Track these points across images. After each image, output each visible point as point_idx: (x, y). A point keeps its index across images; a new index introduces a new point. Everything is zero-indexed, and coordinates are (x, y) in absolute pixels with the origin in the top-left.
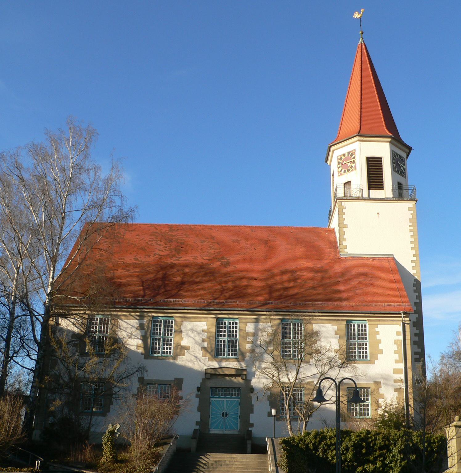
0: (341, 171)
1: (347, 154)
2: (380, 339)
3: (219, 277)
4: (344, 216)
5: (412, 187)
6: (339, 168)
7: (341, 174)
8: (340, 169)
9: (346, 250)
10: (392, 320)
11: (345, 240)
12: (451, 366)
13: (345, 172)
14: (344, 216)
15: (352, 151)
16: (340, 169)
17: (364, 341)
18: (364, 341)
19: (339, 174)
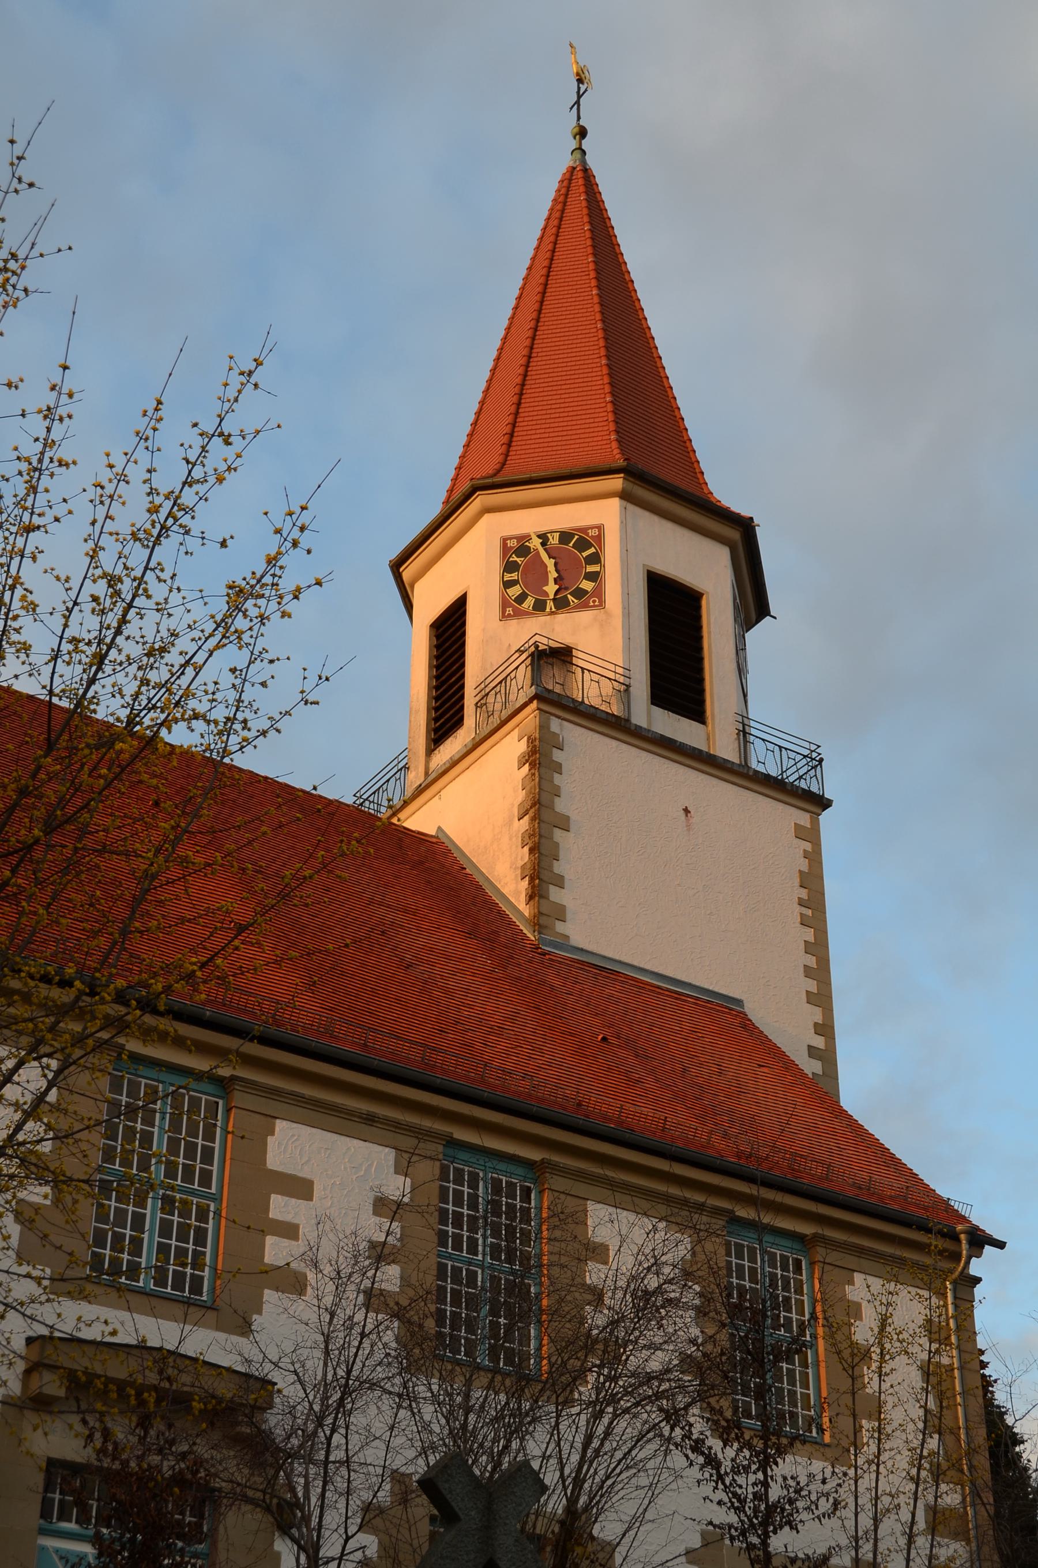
0: (521, 598)
1: (557, 535)
2: (296, 1221)
3: (812, 1322)
4: (557, 779)
5: (807, 745)
6: (507, 585)
7: (518, 614)
8: (515, 591)
9: (560, 927)
10: (751, 1179)
11: (559, 882)
12: (647, 1251)
13: (593, 577)
14: (557, 779)
15: (584, 530)
16: (515, 591)
17: (450, 1257)
18: (450, 1257)
19: (509, 611)
